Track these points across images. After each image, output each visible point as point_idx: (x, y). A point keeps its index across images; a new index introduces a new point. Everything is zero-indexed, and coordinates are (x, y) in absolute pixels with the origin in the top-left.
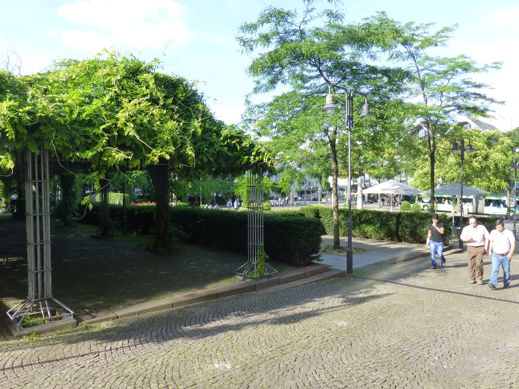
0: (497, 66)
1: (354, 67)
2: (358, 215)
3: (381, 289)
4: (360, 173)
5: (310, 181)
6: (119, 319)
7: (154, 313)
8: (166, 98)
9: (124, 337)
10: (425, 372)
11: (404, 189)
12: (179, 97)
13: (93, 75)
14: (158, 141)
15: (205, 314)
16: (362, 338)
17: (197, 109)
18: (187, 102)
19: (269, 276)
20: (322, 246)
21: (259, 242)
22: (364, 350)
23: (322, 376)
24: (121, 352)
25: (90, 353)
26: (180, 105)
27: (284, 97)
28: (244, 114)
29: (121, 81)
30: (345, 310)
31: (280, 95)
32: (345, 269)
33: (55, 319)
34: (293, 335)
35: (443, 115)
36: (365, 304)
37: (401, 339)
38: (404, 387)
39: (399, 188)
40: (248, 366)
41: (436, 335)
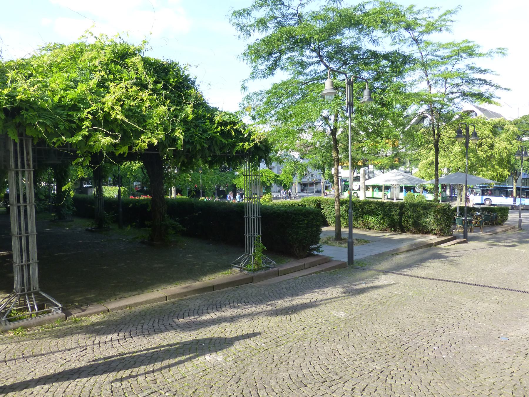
0: (502, 52)
1: (355, 52)
2: (360, 205)
3: (384, 279)
4: (364, 164)
5: (313, 173)
6: (111, 312)
7: (146, 306)
8: (156, 82)
9: (114, 330)
10: (424, 362)
11: (407, 179)
12: (171, 83)
13: (79, 58)
14: (147, 128)
15: (199, 307)
16: (360, 329)
17: (190, 95)
18: (179, 88)
19: (267, 267)
20: (323, 237)
21: (257, 232)
22: (361, 341)
23: (317, 368)
24: (109, 346)
25: (77, 347)
26: (171, 91)
27: (284, 83)
28: (241, 102)
29: (109, 65)
30: (344, 301)
31: (279, 82)
32: (346, 260)
33: (43, 313)
34: (289, 326)
35: (448, 103)
36: (365, 294)
37: (400, 330)
38: (401, 378)
39: (403, 179)
40: (241, 359)
41: (436, 324)
